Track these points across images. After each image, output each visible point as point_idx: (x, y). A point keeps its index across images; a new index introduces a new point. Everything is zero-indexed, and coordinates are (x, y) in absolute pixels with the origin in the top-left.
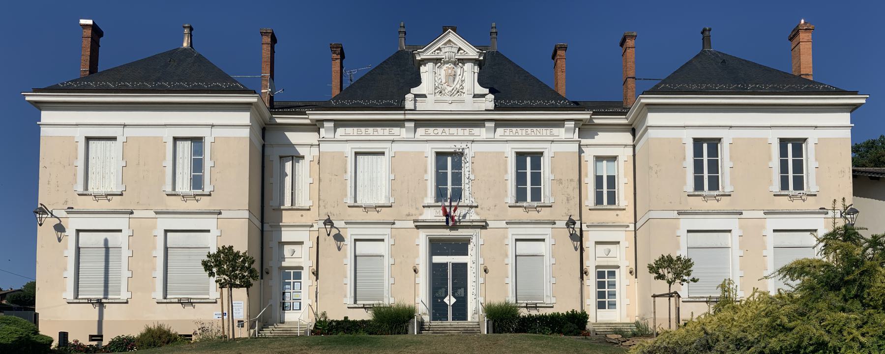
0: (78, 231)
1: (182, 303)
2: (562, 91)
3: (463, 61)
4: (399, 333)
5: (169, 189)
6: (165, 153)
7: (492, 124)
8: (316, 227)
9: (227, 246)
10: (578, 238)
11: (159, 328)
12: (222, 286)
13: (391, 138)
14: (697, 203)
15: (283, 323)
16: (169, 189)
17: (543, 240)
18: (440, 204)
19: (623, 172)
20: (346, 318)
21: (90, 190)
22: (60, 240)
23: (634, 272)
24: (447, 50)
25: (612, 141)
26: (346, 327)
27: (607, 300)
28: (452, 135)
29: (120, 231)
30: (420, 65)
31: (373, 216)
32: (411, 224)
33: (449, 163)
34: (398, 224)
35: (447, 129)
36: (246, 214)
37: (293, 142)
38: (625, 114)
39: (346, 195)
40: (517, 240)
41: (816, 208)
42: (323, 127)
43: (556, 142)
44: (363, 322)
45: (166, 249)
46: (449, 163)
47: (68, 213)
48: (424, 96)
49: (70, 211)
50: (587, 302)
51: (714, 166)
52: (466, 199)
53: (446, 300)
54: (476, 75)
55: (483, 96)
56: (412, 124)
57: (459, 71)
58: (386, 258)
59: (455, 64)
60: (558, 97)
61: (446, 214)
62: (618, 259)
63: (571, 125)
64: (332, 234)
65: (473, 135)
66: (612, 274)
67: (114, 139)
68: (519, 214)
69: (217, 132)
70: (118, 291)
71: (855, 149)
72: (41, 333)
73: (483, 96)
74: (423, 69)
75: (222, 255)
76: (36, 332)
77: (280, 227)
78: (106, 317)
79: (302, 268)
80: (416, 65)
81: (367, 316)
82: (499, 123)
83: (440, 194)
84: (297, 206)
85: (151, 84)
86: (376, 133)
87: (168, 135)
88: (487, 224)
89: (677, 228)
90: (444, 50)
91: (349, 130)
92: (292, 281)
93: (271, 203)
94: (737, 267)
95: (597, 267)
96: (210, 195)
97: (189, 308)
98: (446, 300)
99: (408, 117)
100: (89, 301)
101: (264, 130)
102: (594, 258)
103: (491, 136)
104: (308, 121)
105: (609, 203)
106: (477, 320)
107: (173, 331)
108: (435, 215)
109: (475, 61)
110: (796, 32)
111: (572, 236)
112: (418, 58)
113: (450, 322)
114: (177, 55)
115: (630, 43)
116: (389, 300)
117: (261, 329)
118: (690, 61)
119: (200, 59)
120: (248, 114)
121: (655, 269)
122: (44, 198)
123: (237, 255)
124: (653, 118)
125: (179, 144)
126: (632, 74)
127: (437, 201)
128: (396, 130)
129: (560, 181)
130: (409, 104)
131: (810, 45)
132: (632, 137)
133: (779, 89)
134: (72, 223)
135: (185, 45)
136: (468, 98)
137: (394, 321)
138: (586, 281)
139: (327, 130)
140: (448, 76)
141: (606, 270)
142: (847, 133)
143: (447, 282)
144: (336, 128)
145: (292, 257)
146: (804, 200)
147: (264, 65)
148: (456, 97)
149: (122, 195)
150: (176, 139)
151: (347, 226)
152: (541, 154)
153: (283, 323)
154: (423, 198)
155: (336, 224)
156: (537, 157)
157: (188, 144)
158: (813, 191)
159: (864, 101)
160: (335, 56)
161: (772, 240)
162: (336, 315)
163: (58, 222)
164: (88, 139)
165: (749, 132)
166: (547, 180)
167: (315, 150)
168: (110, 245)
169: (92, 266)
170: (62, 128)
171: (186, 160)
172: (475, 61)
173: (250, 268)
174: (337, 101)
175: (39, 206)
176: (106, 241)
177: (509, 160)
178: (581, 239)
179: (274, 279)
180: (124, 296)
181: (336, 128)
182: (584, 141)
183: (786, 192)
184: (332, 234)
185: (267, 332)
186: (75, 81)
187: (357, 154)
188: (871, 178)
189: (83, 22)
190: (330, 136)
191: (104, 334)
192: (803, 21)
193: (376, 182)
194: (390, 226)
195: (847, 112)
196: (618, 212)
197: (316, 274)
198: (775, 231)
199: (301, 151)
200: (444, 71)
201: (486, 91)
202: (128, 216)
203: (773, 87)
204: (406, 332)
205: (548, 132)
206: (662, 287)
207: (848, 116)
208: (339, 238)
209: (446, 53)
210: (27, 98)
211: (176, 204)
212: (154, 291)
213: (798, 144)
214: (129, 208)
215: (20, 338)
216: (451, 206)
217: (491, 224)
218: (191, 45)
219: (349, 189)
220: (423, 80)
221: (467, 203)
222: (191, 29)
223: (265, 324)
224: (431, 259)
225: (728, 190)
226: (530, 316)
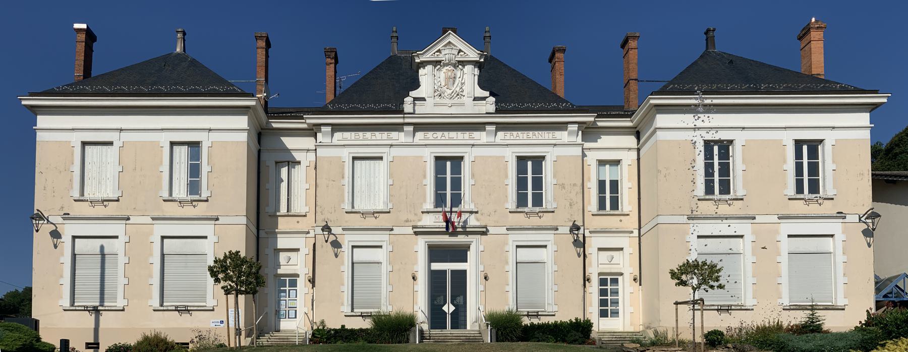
0: (74, 237)
1: (179, 311)
2: (561, 93)
3: (463, 63)
4: (400, 342)
5: (166, 195)
6: (162, 159)
7: (493, 128)
8: (312, 234)
9: (234, 251)
10: (580, 244)
11: (156, 336)
12: (227, 292)
13: (390, 142)
14: (707, 208)
15: (279, 331)
16: (166, 195)
17: (545, 246)
18: (440, 209)
19: (626, 177)
20: (343, 326)
21: (87, 196)
22: (56, 246)
23: (638, 280)
24: (447, 51)
25: (617, 145)
26: (344, 335)
27: (609, 308)
28: (452, 139)
29: (117, 237)
30: (419, 68)
31: (371, 222)
32: (410, 230)
33: (448, 167)
34: (397, 230)
35: (446, 133)
36: (244, 220)
37: (289, 147)
38: (630, 116)
39: (343, 201)
40: (518, 247)
41: (834, 212)
42: (320, 131)
43: (560, 147)
44: (361, 330)
45: (163, 256)
46: (448, 167)
47: (64, 219)
48: (423, 99)
49: (66, 217)
50: (589, 310)
51: (725, 170)
52: (466, 205)
53: (445, 308)
54: (476, 77)
55: (484, 99)
56: (411, 128)
57: (458, 73)
58: (384, 266)
59: (455, 66)
60: (559, 99)
61: (447, 221)
62: (621, 266)
63: (574, 127)
64: (330, 240)
65: (473, 139)
66: (615, 281)
67: (111, 143)
68: (520, 219)
69: (214, 136)
70: (115, 299)
71: (876, 153)
72: (43, 340)
73: (484, 99)
75: (229, 261)
76: (38, 339)
77: (276, 233)
78: (102, 325)
79: (298, 276)
80: (414, 67)
81: (367, 324)
83: (440, 200)
84: (293, 212)
85: (203, 88)
86: (374, 138)
87: (165, 139)
88: (488, 231)
89: (777, 232)
91: (347, 135)
92: (287, 288)
93: (267, 209)
94: (750, 274)
95: (600, 274)
96: (207, 201)
97: (186, 316)
98: (445, 308)
99: (407, 121)
100: (86, 309)
101: (260, 136)
102: (598, 264)
103: (491, 139)
104: (305, 126)
105: (611, 209)
106: (477, 328)
107: (170, 339)
108: (435, 221)
109: (476, 63)
110: (807, 30)
111: (576, 243)
112: (417, 60)
113: (449, 330)
114: (170, 60)
115: (632, 44)
116: (388, 308)
117: (258, 338)
118: (695, 63)
119: (194, 63)
120: (246, 117)
121: (678, 276)
122: (40, 203)
123: (244, 261)
124: (662, 120)
125: (176, 149)
126: (634, 75)
127: (436, 206)
128: (394, 135)
129: (563, 186)
130: (408, 108)
131: (821, 44)
132: (635, 140)
133: (775, 88)
134: (69, 230)
135: (178, 50)
136: (468, 101)
137: (396, 328)
138: (589, 289)
139: (325, 134)
140: (447, 78)
141: (609, 278)
142: (867, 134)
143: (446, 290)
144: (333, 132)
145: (288, 264)
146: (820, 204)
147: (259, 69)
148: (456, 100)
149: (118, 200)
150: (173, 144)
151: (345, 232)
152: (543, 158)
153: (279, 331)
154: (422, 204)
155: (334, 230)
156: (538, 161)
157: (185, 149)
158: (830, 194)
159: (885, 100)
160: (329, 60)
161: (786, 245)
162: (334, 324)
163: (54, 228)
164: (84, 144)
165: (764, 134)
166: (549, 184)
167: (312, 156)
168: (106, 252)
169: (89, 273)
170: (58, 133)
171: (183, 165)
172: (476, 63)
173: (249, 274)
174: (334, 105)
175: (36, 212)
176: (102, 247)
177: (510, 164)
178: (584, 245)
179: (270, 287)
180: (120, 303)
181: (333, 132)
182: (587, 145)
183: (801, 196)
184: (330, 240)
185: (264, 340)
186: (70, 85)
187: (354, 158)
188: (888, 181)
189: (76, 26)
190: (327, 140)
191: (100, 341)
192: (813, 20)
193: (374, 187)
194: (388, 232)
195: (866, 112)
196: (622, 218)
197: (313, 281)
198: (789, 236)
199: (297, 156)
200: (443, 73)
201: (487, 94)
202: (124, 222)
203: (787, 87)
204: (407, 341)
205: (551, 135)
206: (686, 293)
207: (867, 116)
208: (336, 245)
209: (446, 55)
210: (24, 103)
211: (172, 209)
212: (151, 298)
213: (814, 146)
214: (125, 213)
215: (24, 345)
216: (451, 212)
217: (492, 230)
218: (184, 50)
219: (346, 194)
220: (421, 84)
221: (467, 208)
222: (184, 34)
223: (261, 334)
224: (429, 266)
225: (740, 194)
226: (532, 325)
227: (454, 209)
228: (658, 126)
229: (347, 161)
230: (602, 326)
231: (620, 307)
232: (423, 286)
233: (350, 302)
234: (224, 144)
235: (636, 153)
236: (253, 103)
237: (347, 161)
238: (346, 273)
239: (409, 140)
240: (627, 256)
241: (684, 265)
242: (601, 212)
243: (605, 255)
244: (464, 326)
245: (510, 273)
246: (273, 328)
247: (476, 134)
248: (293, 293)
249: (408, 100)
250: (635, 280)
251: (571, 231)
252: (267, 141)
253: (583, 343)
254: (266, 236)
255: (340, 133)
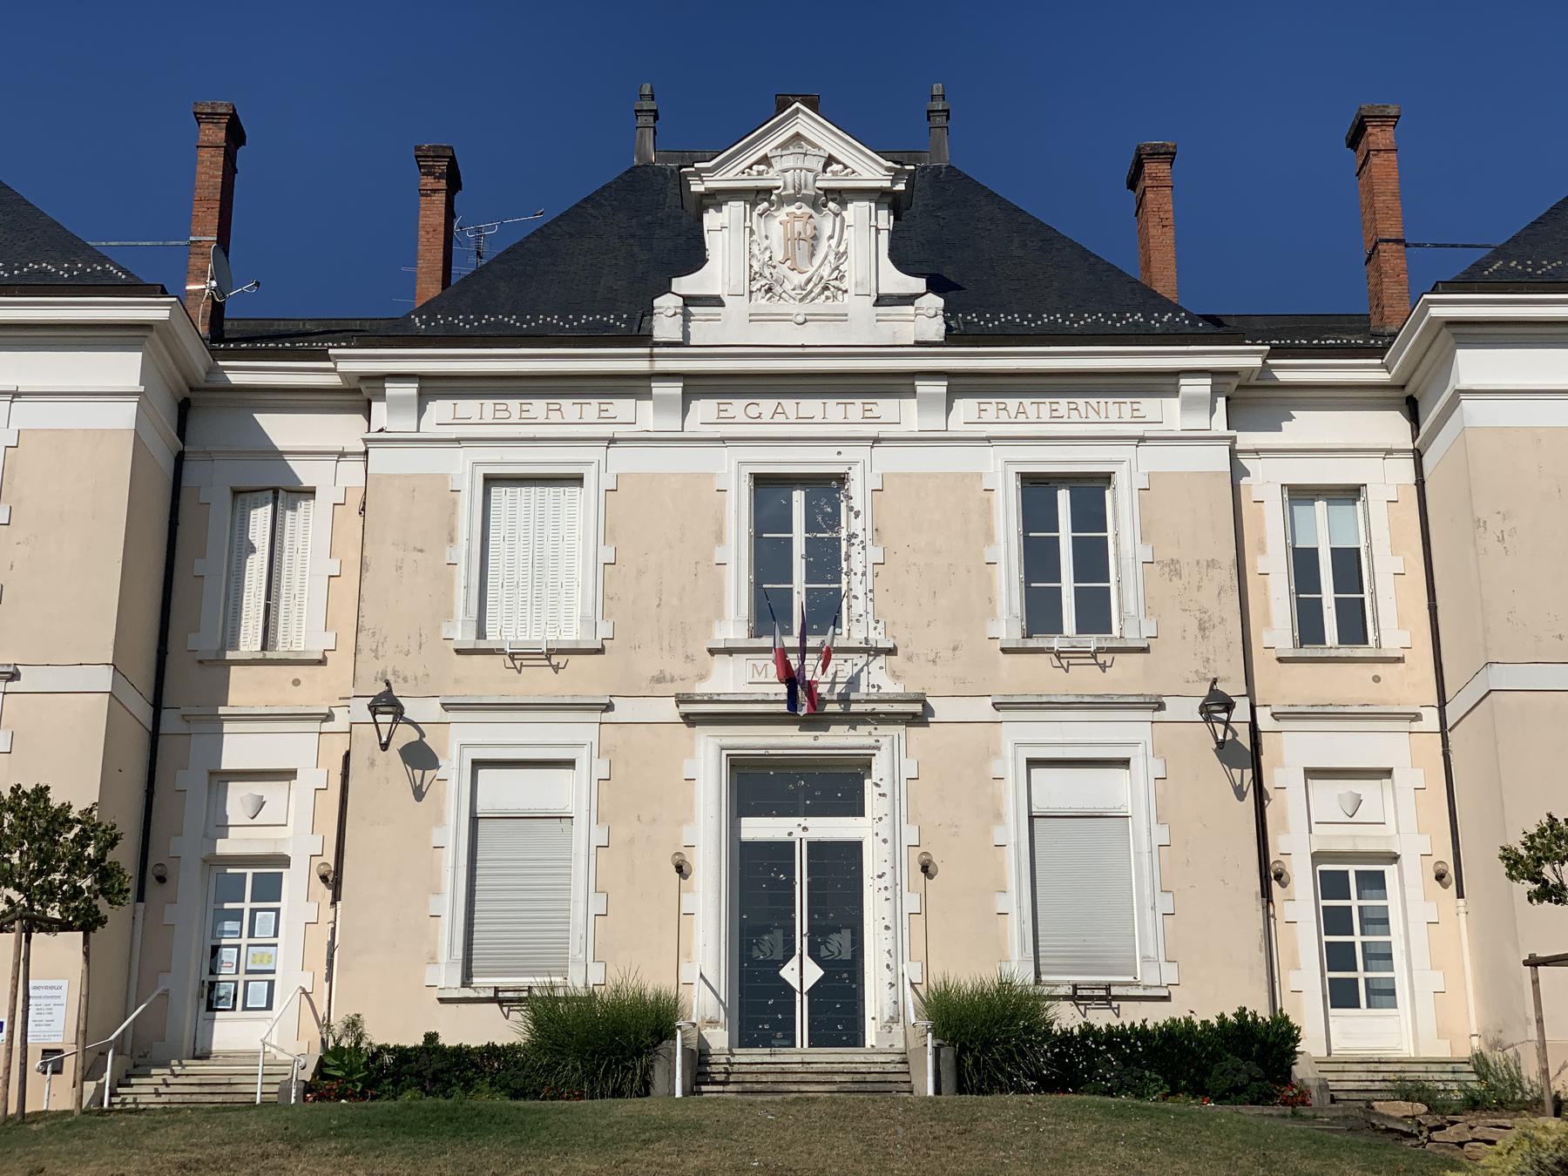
2: (1165, 283)
3: (842, 196)
4: (618, 1093)
8: (341, 721)
9: (28, 787)
10: (1245, 756)
15: (205, 1056)
17: (1125, 763)
18: (767, 642)
20: (431, 1038)
24: (788, 162)
25: (1339, 438)
26: (433, 1069)
30: (705, 209)
31: (539, 683)
32: (670, 710)
34: (624, 710)
35: (789, 404)
37: (281, 443)
38: (1379, 352)
39: (449, 616)
40: (1032, 763)
42: (382, 396)
43: (1156, 444)
44: (491, 1051)
48: (717, 301)
50: (1289, 980)
52: (852, 631)
53: (789, 973)
54: (884, 238)
56: (676, 389)
58: (580, 829)
61: (792, 679)
62: (1391, 828)
63: (1203, 386)
66: (1373, 882)
68: (1037, 675)
74: (710, 219)
77: (219, 720)
79: (284, 861)
80: (690, 207)
82: (962, 384)
83: (769, 611)
84: (280, 651)
86: (555, 417)
90: (778, 165)
91: (469, 407)
93: (190, 641)
95: (1317, 857)
98: (789, 973)
101: (184, 409)
104: (333, 380)
105: (1343, 640)
106: (900, 1045)
108: (751, 679)
109: (879, 196)
111: (1225, 750)
112: (697, 187)
113: (802, 1052)
115: (1378, 136)
116: (589, 966)
117: (121, 1081)
123: (61, 818)
126: (1391, 229)
127: (757, 633)
128: (622, 408)
129: (1173, 568)
130: (665, 325)
132: (1406, 426)
136: (859, 307)
137: (602, 1047)
139: (396, 405)
140: (792, 240)
141: (1352, 869)
143: (792, 909)
147: (199, 209)
148: (820, 305)
151: (451, 716)
152: (1107, 478)
153: (205, 1056)
154: (709, 624)
155: (411, 709)
156: (1091, 490)
160: (429, 182)
162: (394, 1027)
166: (1127, 561)
167: (352, 472)
172: (879, 196)
174: (432, 317)
177: (998, 499)
179: (184, 901)
182: (1246, 439)
184: (399, 741)
185: (143, 1091)
187: (490, 481)
190: (404, 424)
193: (552, 570)
194: (597, 716)
196: (1379, 669)
197: (334, 881)
199: (306, 473)
200: (778, 226)
201: (919, 284)
204: (645, 1089)
208: (420, 757)
209: (785, 172)
216: (803, 651)
217: (942, 709)
219: (460, 594)
223: (139, 1058)
224: (734, 829)
226: (1088, 1031)
227: (813, 642)
228: (1465, 383)
229: (466, 487)
230: (1333, 1040)
231: (1399, 974)
232: (711, 897)
233: (459, 953)
234: (60, 436)
235: (1410, 464)
236: (162, 314)
237: (466, 487)
238: (448, 853)
239: (671, 423)
240: (1407, 799)
241: (1542, 832)
242: (1308, 651)
243: (1329, 794)
244: (854, 1037)
245: (1010, 852)
246: (187, 1046)
247: (886, 407)
248: (265, 920)
249: (666, 304)
250: (1440, 877)
251: (1205, 710)
252: (208, 428)
253: (1264, 1098)
254: (182, 727)
255: (448, 403)
